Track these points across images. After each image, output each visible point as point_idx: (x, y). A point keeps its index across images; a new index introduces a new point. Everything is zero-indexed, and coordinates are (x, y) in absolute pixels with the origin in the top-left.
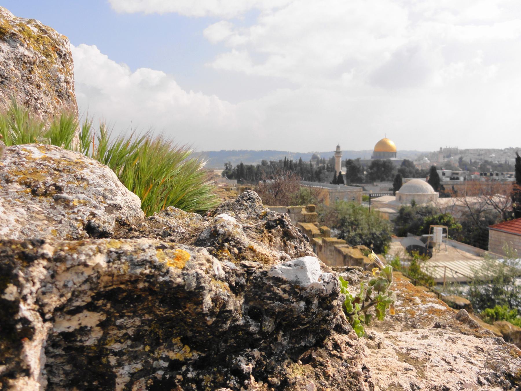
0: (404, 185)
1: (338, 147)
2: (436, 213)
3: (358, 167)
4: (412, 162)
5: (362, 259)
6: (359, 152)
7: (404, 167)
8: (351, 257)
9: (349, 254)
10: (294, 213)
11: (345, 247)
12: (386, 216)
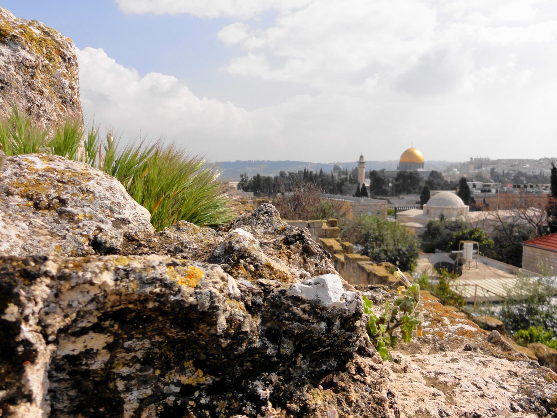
0: (432, 198)
1: (361, 157)
3: (383, 178)
5: (387, 277)
6: (384, 163)
7: (431, 178)
8: (375, 275)
9: (373, 272)
10: (314, 228)
12: (413, 231)
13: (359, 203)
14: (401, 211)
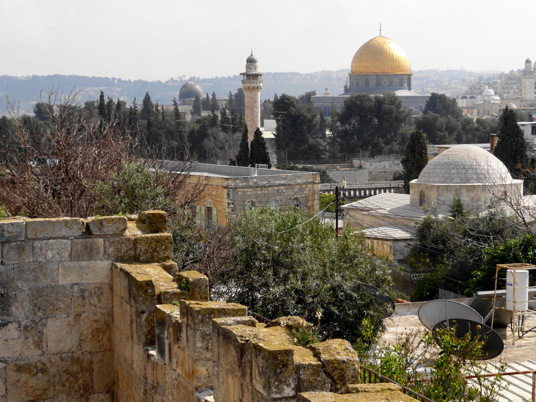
0: (432, 162)
1: (251, 61)
2: (514, 234)
3: (309, 116)
4: (454, 101)
5: (289, 353)
6: (313, 76)
7: (431, 114)
8: (258, 349)
9: (254, 341)
10: (104, 236)
11: (244, 323)
12: (386, 249)
13: (246, 180)
14: (354, 198)
